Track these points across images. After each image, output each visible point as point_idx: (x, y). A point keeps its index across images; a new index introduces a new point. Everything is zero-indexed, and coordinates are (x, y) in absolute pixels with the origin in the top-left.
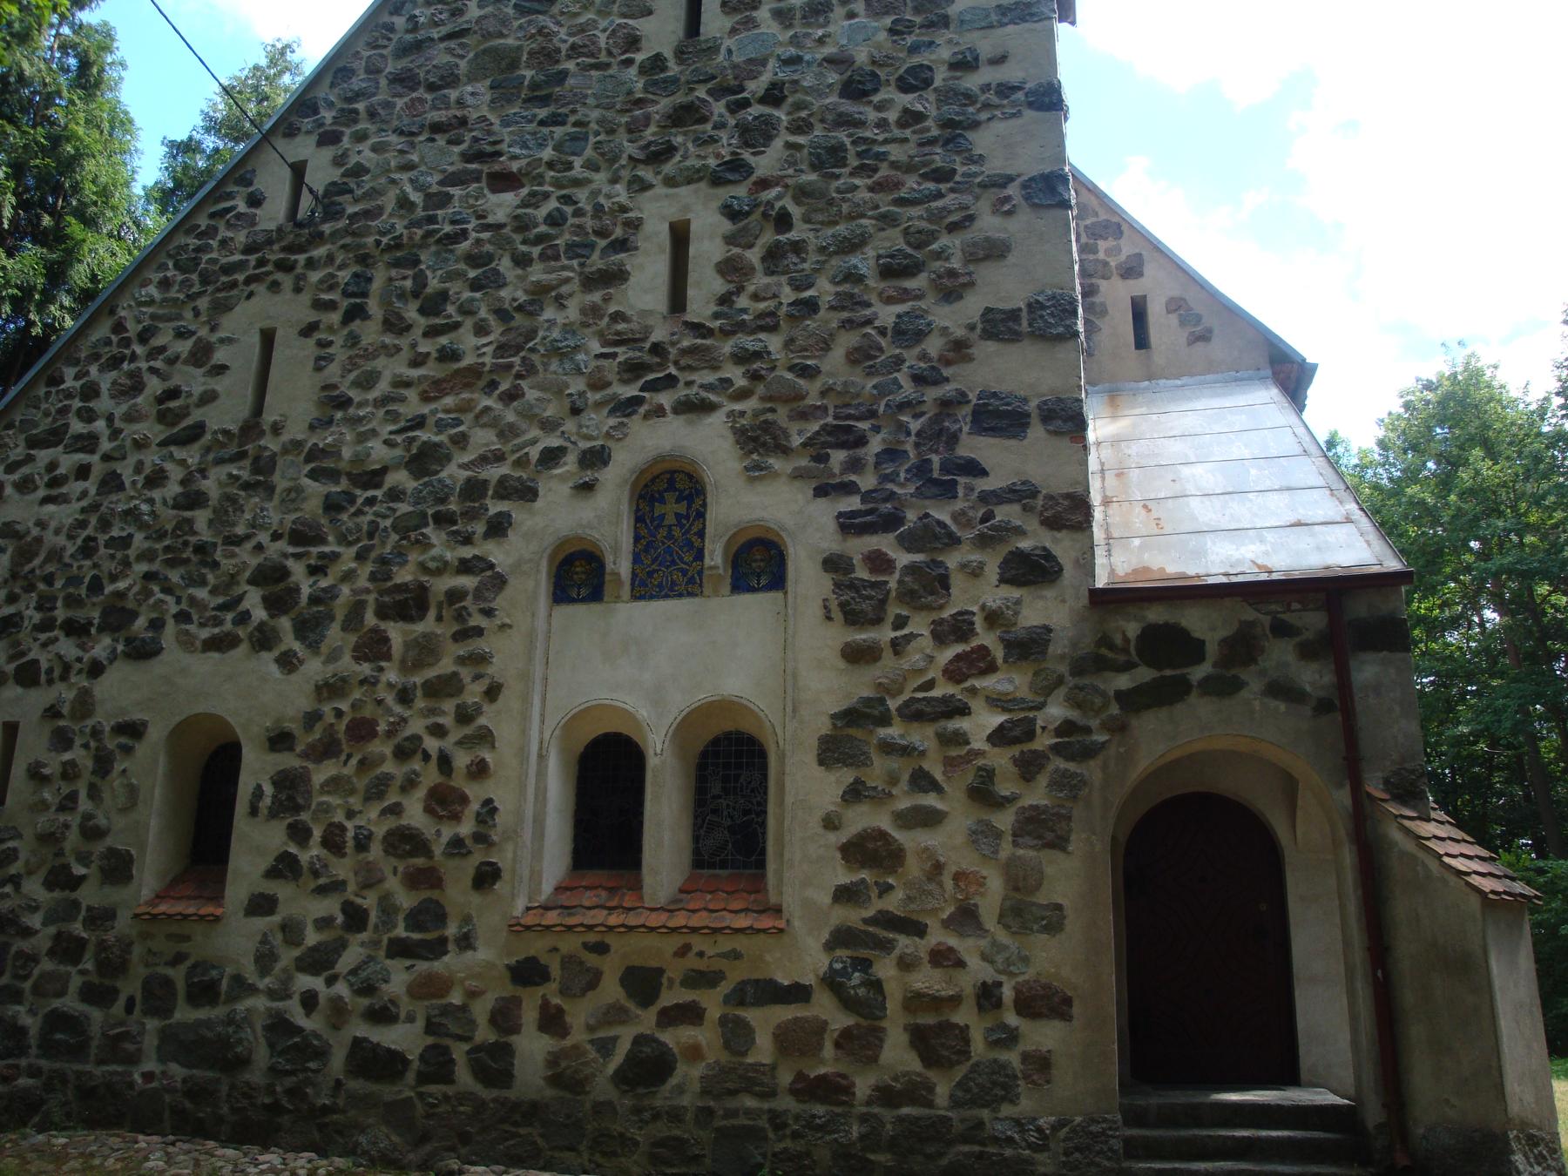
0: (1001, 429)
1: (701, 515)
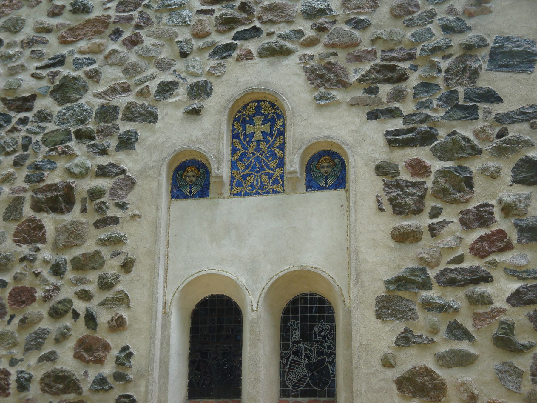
0: (513, 66)
1: (281, 133)
